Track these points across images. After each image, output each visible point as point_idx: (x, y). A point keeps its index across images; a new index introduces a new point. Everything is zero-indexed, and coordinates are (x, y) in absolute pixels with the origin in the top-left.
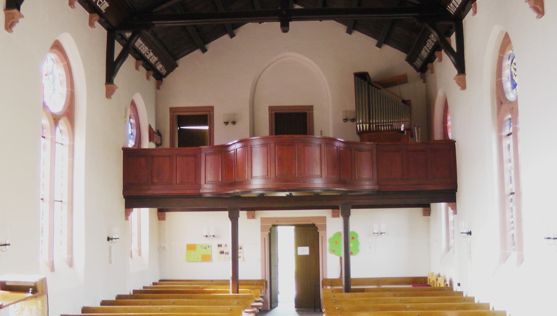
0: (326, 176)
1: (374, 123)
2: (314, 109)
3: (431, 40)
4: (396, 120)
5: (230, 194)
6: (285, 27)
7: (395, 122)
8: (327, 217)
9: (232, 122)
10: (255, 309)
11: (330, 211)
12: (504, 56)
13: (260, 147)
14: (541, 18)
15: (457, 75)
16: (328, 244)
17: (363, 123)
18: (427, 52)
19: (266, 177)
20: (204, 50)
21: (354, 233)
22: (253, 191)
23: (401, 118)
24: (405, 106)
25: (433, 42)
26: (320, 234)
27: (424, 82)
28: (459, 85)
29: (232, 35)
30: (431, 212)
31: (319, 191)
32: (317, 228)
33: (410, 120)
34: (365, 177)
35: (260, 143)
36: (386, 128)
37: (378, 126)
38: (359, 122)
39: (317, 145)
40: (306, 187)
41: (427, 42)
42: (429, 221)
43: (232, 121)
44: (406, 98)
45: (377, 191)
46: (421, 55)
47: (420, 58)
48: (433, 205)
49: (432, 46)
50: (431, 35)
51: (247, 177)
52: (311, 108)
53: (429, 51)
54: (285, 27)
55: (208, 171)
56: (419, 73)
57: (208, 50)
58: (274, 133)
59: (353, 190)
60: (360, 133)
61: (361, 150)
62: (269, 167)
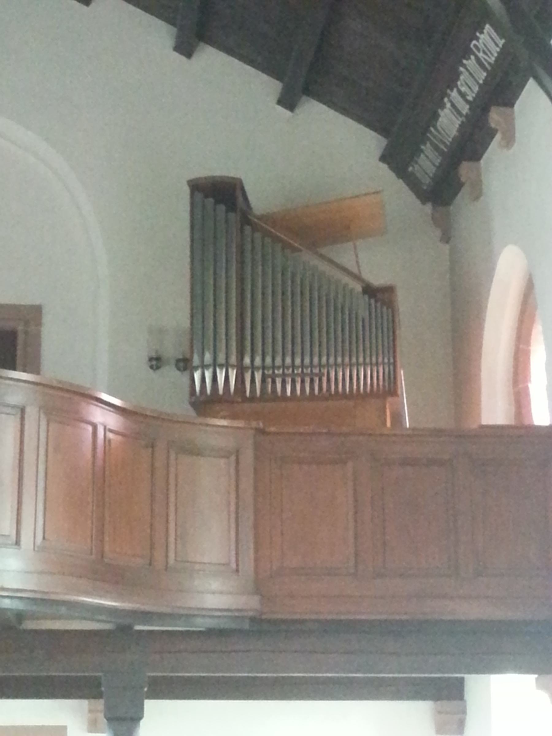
1: (258, 368)
2: (47, 319)
3: (478, 60)
17: (215, 364)
18: (459, 113)
24: (373, 306)
27: (446, 238)
30: (468, 718)
33: (392, 361)
41: (461, 69)
45: (253, 620)
47: (432, 144)
49: (480, 86)
50: (477, 39)
53: (465, 109)
56: (428, 208)
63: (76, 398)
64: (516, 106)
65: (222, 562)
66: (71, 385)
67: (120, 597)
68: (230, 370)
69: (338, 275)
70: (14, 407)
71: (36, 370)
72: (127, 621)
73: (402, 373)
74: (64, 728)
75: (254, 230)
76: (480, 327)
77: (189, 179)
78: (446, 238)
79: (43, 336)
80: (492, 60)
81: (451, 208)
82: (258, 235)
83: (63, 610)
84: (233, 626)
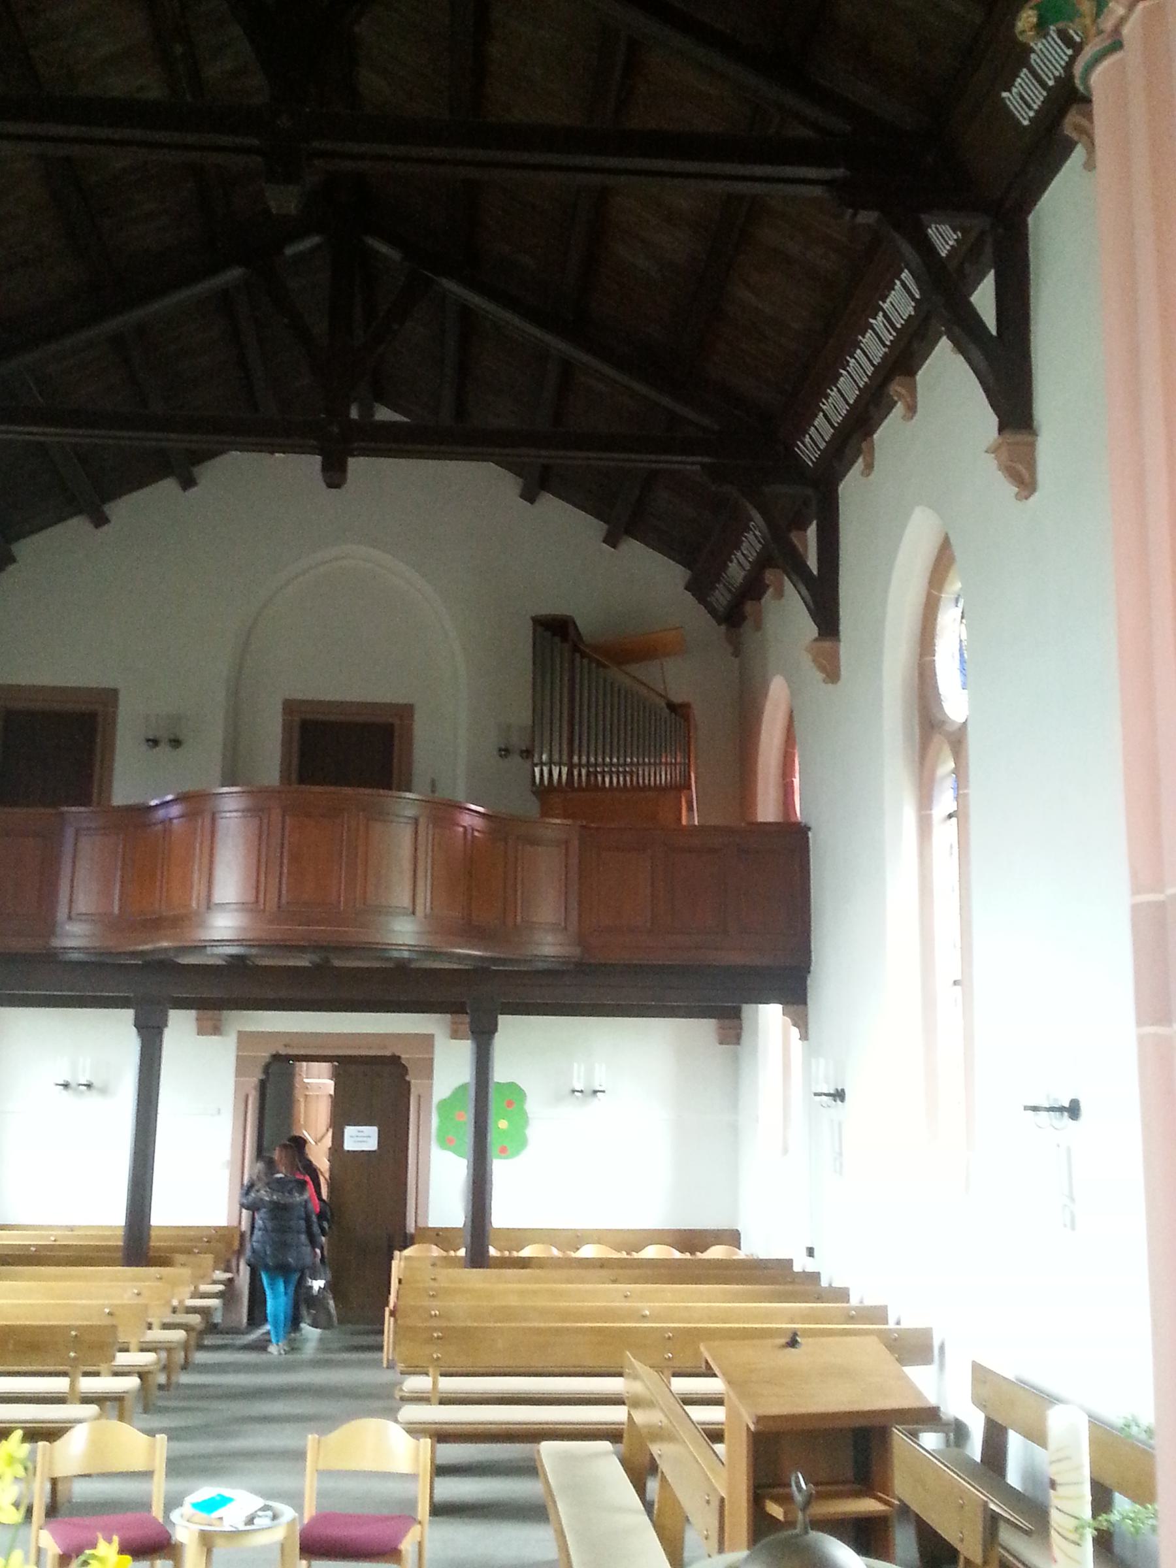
0: (428, 910)
2: (418, 717)
4: (647, 760)
5: (142, 953)
6: (334, 474)
7: (644, 764)
8: (436, 1036)
9: (170, 741)
10: (195, 1319)
12: (943, 595)
13: (240, 817)
14: (1026, 498)
15: (816, 640)
17: (551, 763)
19: (253, 907)
20: (100, 520)
21: (513, 1087)
22: (210, 946)
23: (611, 751)
26: (413, 1090)
28: (822, 668)
29: (188, 483)
31: (406, 955)
32: (407, 1070)
35: (241, 806)
36: (632, 780)
37: (596, 773)
38: (541, 758)
39: (405, 820)
42: (736, 1059)
43: (172, 737)
44: (677, 699)
45: (578, 964)
46: (726, 574)
47: (724, 585)
48: (747, 1009)
51: (194, 905)
52: (406, 712)
54: (334, 474)
56: (723, 627)
57: (113, 522)
58: (294, 776)
59: (514, 957)
60: (544, 793)
61: (534, 842)
62: (262, 879)
67: (485, 950)
68: (562, 767)
74: (433, 1035)
75: (582, 657)
78: (737, 652)
82: (585, 661)
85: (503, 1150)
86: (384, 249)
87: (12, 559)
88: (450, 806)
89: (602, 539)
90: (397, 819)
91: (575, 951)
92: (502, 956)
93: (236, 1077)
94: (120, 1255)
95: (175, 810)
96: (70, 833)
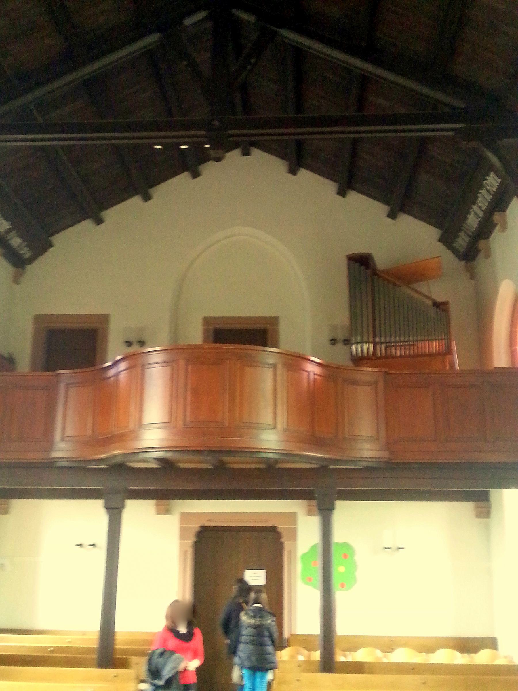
11: (304, 502)
16: (299, 566)
20: (99, 221)
21: (346, 545)
25: (491, 194)
31: (271, 456)
34: (364, 434)
39: (269, 366)
40: (244, 446)
42: (487, 528)
45: (387, 462)
47: (465, 232)
53: (481, 214)
55: (69, 419)
56: (463, 263)
61: (354, 383)
63: (299, 359)
64: (508, 212)
65: (369, 435)
66: (295, 353)
69: (421, 297)
70: (271, 364)
71: (275, 346)
72: (325, 463)
73: (454, 343)
76: (491, 321)
77: (347, 254)
78: (473, 275)
79: (99, 313)
80: (495, 189)
81: (475, 263)
83: (297, 459)
84: (375, 466)
85: (343, 585)
86: (245, 16)
87: (51, 246)
88: (299, 357)
89: (386, 214)
90: (261, 365)
91: (384, 455)
92: (334, 457)
93: (180, 540)
94: (95, 656)
95: (123, 366)
96: (62, 387)
